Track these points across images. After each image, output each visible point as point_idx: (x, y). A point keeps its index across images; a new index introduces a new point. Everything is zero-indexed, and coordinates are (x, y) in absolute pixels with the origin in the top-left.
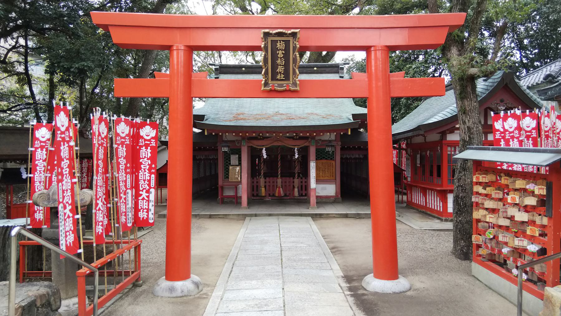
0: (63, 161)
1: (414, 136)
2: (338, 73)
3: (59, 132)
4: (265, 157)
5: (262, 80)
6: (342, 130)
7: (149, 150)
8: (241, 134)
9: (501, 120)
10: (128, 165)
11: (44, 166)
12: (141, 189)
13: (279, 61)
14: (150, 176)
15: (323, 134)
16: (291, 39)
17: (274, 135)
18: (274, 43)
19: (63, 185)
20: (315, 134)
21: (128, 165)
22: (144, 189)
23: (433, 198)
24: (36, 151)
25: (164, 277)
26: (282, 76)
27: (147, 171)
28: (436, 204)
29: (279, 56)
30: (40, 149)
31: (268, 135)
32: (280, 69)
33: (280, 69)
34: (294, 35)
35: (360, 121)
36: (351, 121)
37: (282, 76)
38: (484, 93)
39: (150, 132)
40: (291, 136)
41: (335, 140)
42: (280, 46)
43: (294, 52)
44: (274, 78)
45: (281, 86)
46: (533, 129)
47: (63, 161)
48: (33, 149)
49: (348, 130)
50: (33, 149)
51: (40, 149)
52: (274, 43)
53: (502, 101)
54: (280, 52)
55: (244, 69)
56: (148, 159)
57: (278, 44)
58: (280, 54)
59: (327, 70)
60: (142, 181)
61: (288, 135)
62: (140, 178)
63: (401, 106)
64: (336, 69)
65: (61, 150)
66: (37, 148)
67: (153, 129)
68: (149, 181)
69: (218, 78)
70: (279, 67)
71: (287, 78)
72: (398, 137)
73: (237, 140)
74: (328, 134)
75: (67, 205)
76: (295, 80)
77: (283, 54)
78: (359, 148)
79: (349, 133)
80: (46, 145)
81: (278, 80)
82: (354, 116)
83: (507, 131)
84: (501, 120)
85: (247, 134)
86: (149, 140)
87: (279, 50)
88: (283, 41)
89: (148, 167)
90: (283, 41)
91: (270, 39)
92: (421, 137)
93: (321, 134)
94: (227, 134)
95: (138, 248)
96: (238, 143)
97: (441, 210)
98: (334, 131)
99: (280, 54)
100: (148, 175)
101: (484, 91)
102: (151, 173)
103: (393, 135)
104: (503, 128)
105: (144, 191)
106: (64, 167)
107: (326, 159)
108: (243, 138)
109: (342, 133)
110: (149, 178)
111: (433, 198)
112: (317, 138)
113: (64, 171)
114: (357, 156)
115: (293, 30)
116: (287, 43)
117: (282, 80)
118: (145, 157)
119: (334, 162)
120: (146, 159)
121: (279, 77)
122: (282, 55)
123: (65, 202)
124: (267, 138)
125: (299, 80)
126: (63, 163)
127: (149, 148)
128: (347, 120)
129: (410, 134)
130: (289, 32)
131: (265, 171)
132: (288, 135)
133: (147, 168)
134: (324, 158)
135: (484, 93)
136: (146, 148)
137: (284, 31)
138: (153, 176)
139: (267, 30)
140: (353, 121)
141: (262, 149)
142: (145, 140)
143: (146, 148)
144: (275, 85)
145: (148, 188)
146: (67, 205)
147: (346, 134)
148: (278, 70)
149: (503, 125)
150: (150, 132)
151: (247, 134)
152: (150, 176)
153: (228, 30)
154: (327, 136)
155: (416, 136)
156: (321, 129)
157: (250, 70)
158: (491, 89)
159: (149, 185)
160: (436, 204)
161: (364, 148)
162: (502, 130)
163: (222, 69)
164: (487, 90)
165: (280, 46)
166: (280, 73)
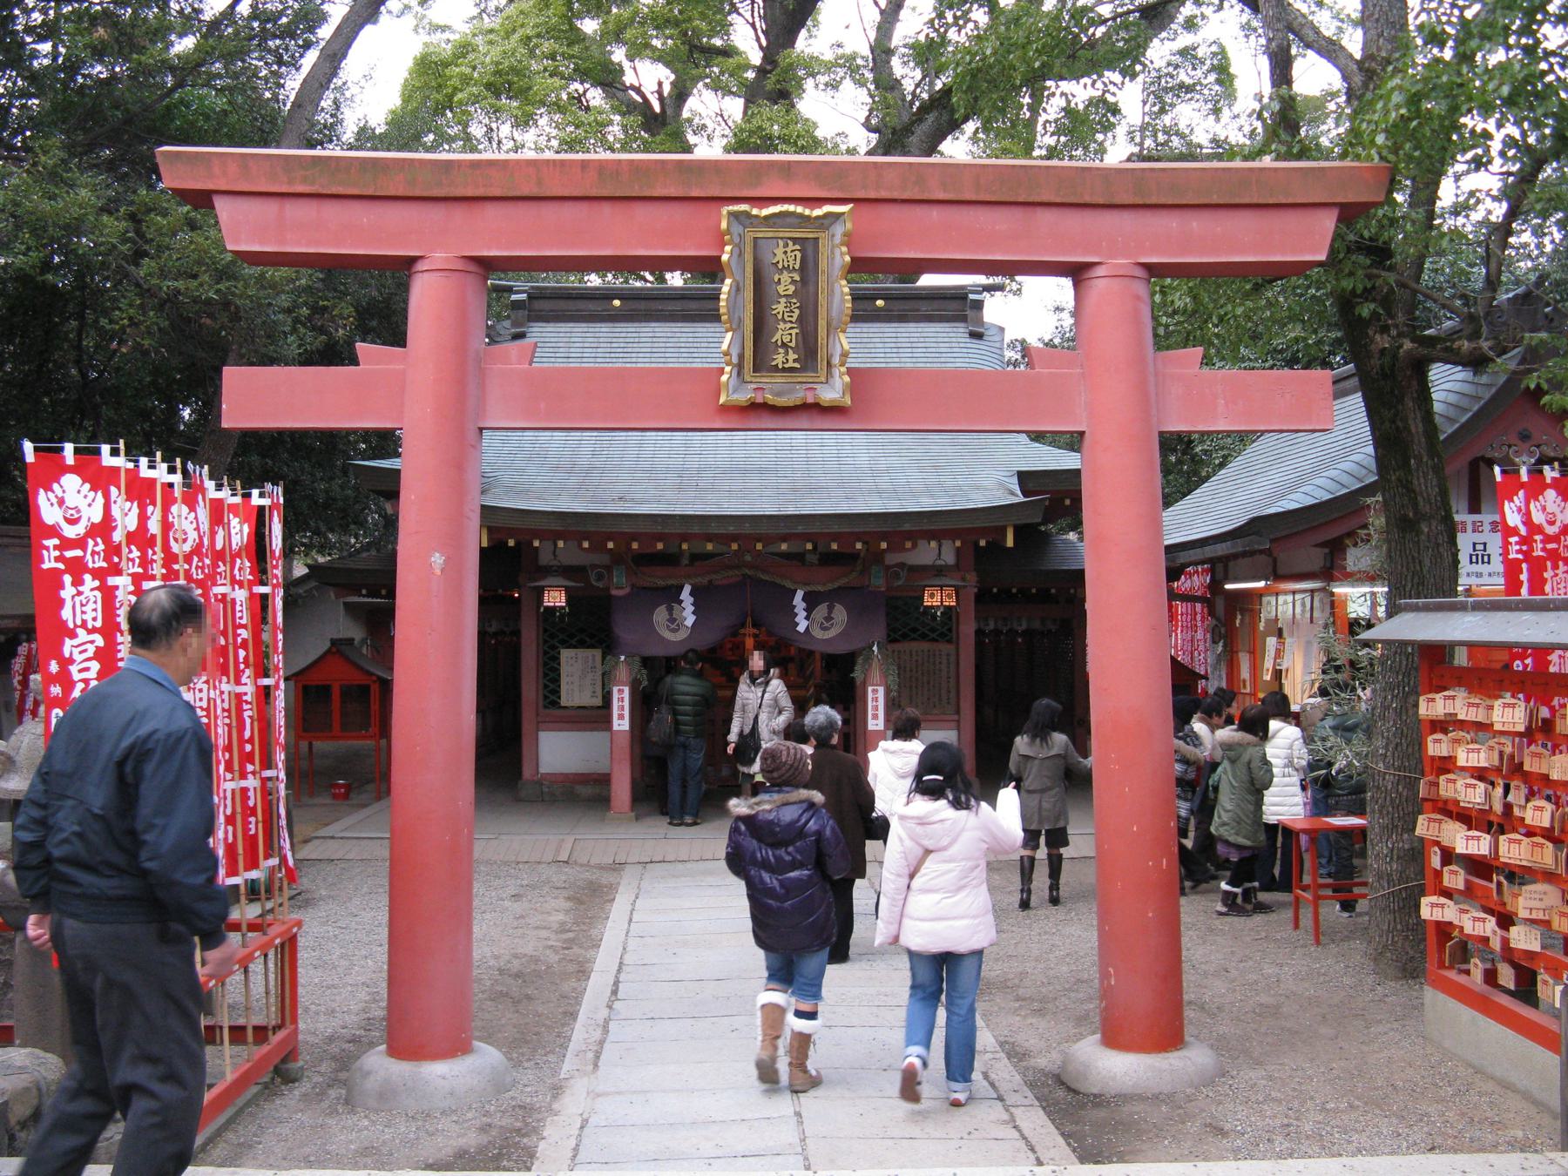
0: (73, 635)
1: (1235, 556)
2: (964, 319)
3: (51, 543)
4: (1227, 587)
5: (721, 371)
6: (983, 531)
8: (610, 545)
9: (1521, 493)
13: (780, 308)
15: (914, 546)
17: (735, 546)
20: (884, 545)
25: (383, 1047)
26: (792, 356)
31: (710, 547)
32: (785, 332)
33: (785, 332)
35: (1055, 499)
36: (1016, 500)
37: (792, 356)
38: (1465, 410)
40: (795, 549)
41: (957, 566)
42: (784, 255)
47: (73, 635)
49: (1003, 530)
53: (1525, 437)
54: (785, 277)
55: (617, 303)
58: (785, 284)
59: (924, 307)
61: (784, 547)
63: (1184, 462)
64: (954, 305)
65: (62, 602)
69: (521, 336)
70: (782, 326)
72: (1184, 557)
73: (594, 566)
74: (933, 544)
77: (793, 282)
78: (1044, 597)
79: (1010, 543)
81: (776, 369)
82: (1023, 477)
83: (1539, 529)
84: (1521, 493)
85: (635, 546)
87: (781, 271)
92: (1263, 557)
93: (908, 545)
94: (561, 544)
95: (289, 947)
96: (600, 577)
98: (952, 534)
99: (785, 284)
101: (1465, 403)
103: (1170, 549)
104: (1528, 521)
106: (78, 657)
107: (924, 637)
108: (617, 558)
109: (983, 543)
112: (891, 559)
113: (74, 669)
114: (1037, 625)
117: (792, 370)
119: (951, 648)
121: (779, 359)
122: (792, 288)
124: (710, 556)
126: (68, 643)
128: (999, 493)
129: (1221, 549)
131: (710, 681)
132: (784, 547)
134: (914, 630)
135: (1465, 410)
137: (799, 209)
140: (1021, 499)
141: (682, 588)
144: (773, 389)
147: (996, 546)
148: (777, 336)
149: (1528, 514)
151: (635, 546)
154: (925, 554)
155: (1244, 554)
156: (907, 527)
157: (642, 305)
158: (1487, 396)
161: (1066, 595)
162: (1523, 531)
163: (538, 305)
164: (1476, 398)
166: (784, 345)
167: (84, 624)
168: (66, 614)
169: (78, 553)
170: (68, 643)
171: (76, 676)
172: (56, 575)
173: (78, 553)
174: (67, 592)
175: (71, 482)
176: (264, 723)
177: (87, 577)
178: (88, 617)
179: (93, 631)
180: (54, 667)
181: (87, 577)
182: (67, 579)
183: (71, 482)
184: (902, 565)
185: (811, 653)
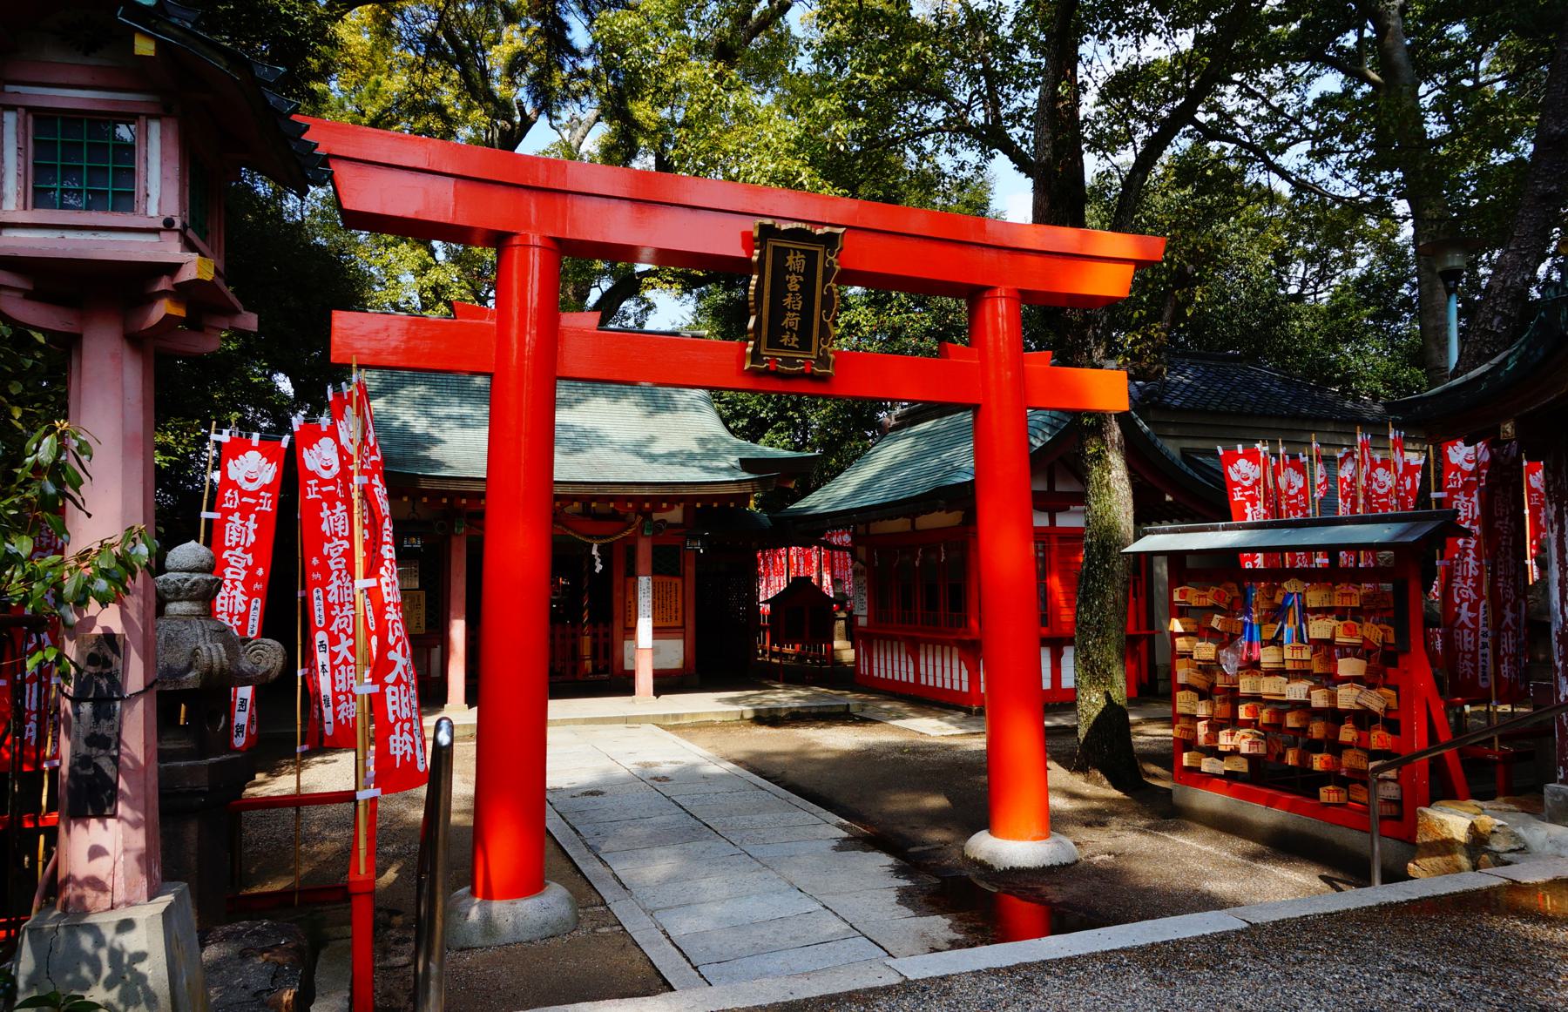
7: (252, 525)
10: (260, 572)
11: (246, 567)
12: (1457, 600)
13: (788, 301)
14: (248, 604)
16: (820, 250)
18: (780, 254)
19: (326, 593)
21: (260, 572)
22: (1463, 600)
23: (938, 663)
24: (224, 520)
26: (795, 339)
27: (241, 588)
28: (947, 674)
29: (790, 286)
30: (237, 515)
32: (791, 320)
33: (791, 320)
34: (830, 240)
39: (261, 470)
42: (795, 262)
43: (826, 280)
44: (774, 343)
45: (790, 361)
46: (265, 488)
47: (330, 541)
48: (216, 515)
50: (216, 515)
51: (237, 515)
52: (780, 254)
54: (794, 277)
56: (246, 551)
57: (790, 258)
58: (793, 283)
60: (224, 616)
62: (219, 609)
66: (231, 512)
67: (270, 461)
68: (244, 617)
71: (805, 345)
75: (342, 636)
76: (825, 351)
80: (258, 504)
86: (255, 495)
88: (803, 252)
89: (244, 573)
90: (803, 252)
91: (771, 244)
97: (965, 688)
99: (793, 283)
100: (240, 598)
102: (250, 593)
105: (1465, 605)
110: (243, 609)
111: (938, 663)
112: (656, 516)
113: (331, 562)
115: (827, 229)
116: (811, 258)
118: (238, 544)
120: (238, 551)
121: (785, 339)
123: (334, 628)
125: (834, 352)
126: (327, 546)
127: (253, 517)
130: (819, 232)
133: (242, 578)
136: (245, 518)
138: (257, 603)
139: (768, 221)
142: (243, 493)
143: (245, 518)
145: (1474, 597)
146: (342, 636)
150: (261, 470)
152: (248, 604)
153: (688, 211)
159: (1477, 590)
160: (947, 674)
165: (795, 262)
166: (790, 329)
167: (336, 534)
168: (325, 527)
169: (332, 488)
170: (327, 546)
171: (333, 567)
172: (317, 503)
173: (332, 488)
174: (325, 513)
175: (1242, 463)
176: (380, 611)
177: (338, 504)
178: (339, 529)
179: (343, 538)
180: (315, 561)
181: (338, 504)
182: (325, 505)
183: (1242, 463)
184: (664, 521)
185: (159, 751)
